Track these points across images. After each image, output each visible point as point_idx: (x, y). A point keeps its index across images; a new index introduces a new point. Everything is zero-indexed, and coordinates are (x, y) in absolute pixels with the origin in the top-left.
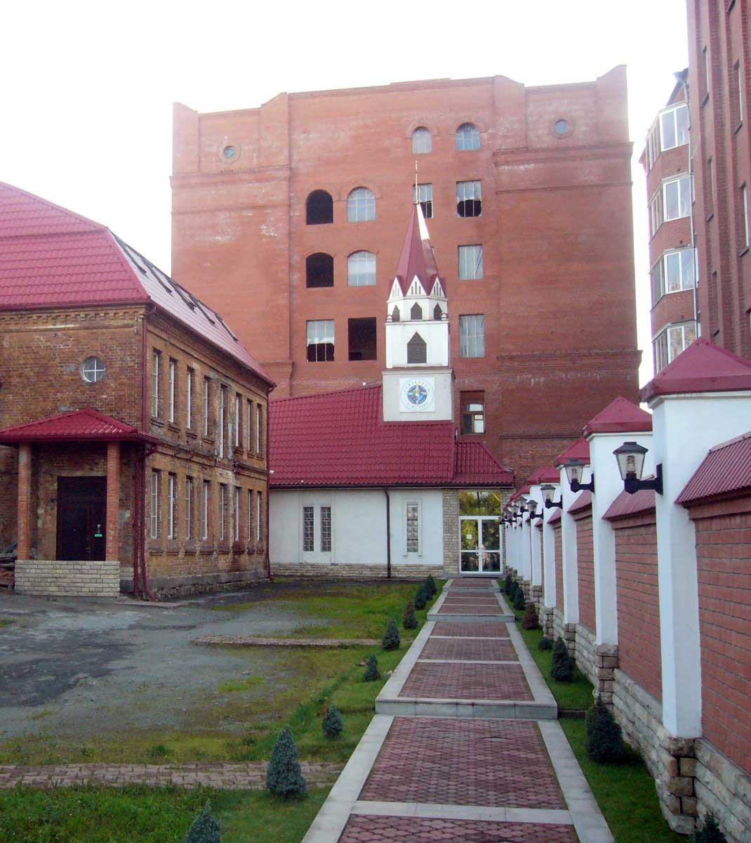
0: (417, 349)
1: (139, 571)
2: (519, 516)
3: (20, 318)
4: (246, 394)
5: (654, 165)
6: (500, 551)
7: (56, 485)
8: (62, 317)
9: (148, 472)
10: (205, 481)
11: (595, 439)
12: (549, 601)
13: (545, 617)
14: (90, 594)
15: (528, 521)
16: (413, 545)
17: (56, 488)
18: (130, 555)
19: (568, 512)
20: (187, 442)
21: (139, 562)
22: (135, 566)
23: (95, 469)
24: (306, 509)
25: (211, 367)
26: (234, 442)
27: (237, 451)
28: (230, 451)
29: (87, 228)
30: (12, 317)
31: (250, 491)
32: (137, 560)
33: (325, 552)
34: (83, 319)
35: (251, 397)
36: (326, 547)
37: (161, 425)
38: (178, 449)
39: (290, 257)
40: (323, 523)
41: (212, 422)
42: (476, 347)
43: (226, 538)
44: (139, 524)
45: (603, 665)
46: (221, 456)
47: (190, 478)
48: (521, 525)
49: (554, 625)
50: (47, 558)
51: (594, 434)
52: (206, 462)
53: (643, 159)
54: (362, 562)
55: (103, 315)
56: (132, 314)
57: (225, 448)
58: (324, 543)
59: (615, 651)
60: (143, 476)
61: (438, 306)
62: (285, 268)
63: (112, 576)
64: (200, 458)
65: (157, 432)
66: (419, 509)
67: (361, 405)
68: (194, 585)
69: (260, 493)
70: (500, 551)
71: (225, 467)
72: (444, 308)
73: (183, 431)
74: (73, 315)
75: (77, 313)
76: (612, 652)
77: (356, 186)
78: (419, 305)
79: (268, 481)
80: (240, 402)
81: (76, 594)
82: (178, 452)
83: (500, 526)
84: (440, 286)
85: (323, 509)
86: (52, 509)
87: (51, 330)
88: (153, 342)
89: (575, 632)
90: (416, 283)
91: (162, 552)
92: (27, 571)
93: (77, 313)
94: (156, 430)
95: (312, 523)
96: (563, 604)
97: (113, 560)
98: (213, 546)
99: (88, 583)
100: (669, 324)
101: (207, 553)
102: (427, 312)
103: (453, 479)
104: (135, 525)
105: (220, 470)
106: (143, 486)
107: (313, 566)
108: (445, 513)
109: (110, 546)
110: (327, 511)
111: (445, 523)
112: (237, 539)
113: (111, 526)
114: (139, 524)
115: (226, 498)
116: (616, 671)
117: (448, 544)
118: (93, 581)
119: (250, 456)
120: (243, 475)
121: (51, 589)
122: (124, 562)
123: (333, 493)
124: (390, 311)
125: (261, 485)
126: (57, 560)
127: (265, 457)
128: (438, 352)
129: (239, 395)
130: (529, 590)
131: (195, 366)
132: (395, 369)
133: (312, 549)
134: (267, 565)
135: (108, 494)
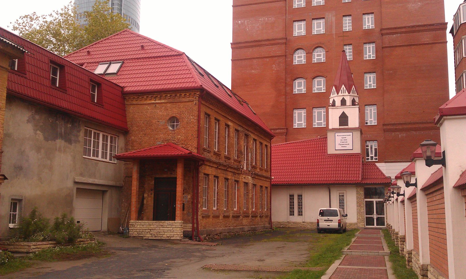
0: (344, 119)
1: (195, 226)
2: (392, 197)
3: (138, 98)
4: (259, 140)
5: (463, 75)
6: (385, 216)
7: (153, 181)
8: (158, 97)
9: (201, 175)
10: (235, 181)
12: (409, 246)
13: (407, 255)
14: (167, 238)
15: (397, 200)
17: (154, 183)
18: (190, 218)
19: (421, 189)
20: (225, 161)
21: (195, 221)
22: (193, 223)
23: (174, 174)
24: (290, 196)
25: (239, 125)
26: (252, 163)
27: (254, 167)
28: (250, 166)
29: (173, 53)
30: (134, 97)
31: (261, 187)
32: (194, 220)
34: (169, 98)
35: (261, 141)
36: (300, 214)
37: (209, 152)
38: (219, 164)
39: (286, 80)
40: (299, 203)
41: (240, 152)
42: (372, 120)
43: (248, 208)
44: (195, 201)
46: (245, 168)
47: (227, 179)
48: (393, 202)
49: (413, 260)
50: (148, 219)
51: (445, 117)
52: (236, 171)
53: (452, 32)
55: (179, 95)
56: (193, 94)
57: (247, 165)
58: (299, 212)
60: (198, 177)
61: (354, 99)
62: (284, 85)
63: (178, 229)
64: (232, 170)
65: (207, 155)
66: (345, 196)
67: (335, 163)
68: (229, 232)
69: (267, 188)
71: (246, 174)
72: (357, 100)
73: (222, 156)
74: (164, 95)
75: (166, 95)
79: (271, 182)
80: (256, 143)
81: (160, 238)
82: (218, 166)
84: (354, 89)
86: (151, 194)
87: (153, 103)
88: (204, 109)
90: (343, 88)
91: (209, 216)
92: (136, 226)
93: (166, 95)
94: (206, 154)
96: (418, 249)
97: (179, 220)
98: (240, 213)
99: (166, 232)
101: (236, 217)
102: (349, 102)
104: (193, 202)
105: (244, 176)
106: (198, 182)
109: (178, 212)
110: (300, 197)
112: (254, 210)
113: (179, 202)
114: (195, 201)
115: (247, 190)
117: (359, 213)
118: (169, 231)
119: (261, 169)
120: (207, 165)
121: (147, 235)
122: (185, 221)
124: (331, 101)
125: (267, 184)
126: (153, 220)
127: (269, 170)
128: (354, 122)
129: (255, 140)
131: (230, 123)
132: (334, 130)
133: (293, 215)
134: (270, 222)
135: (177, 186)
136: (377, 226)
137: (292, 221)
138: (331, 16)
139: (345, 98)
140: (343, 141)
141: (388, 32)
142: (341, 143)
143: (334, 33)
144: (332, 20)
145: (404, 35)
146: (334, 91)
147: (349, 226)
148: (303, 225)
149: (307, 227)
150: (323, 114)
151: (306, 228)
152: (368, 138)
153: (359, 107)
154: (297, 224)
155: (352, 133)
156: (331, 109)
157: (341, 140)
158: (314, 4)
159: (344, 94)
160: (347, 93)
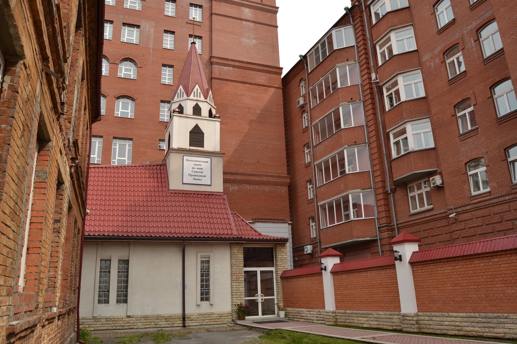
16: (205, 296)
33: (121, 305)
72: (214, 112)
78: (199, 126)
90: (181, 90)
100: (346, 146)
102: (205, 112)
107: (107, 319)
133: (107, 302)
136: (262, 315)
137: (103, 315)
138: (147, 26)
139: (200, 104)
140: (196, 170)
141: (219, 62)
142: (192, 174)
143: (152, 47)
144: (149, 31)
145: (236, 69)
146: (182, 92)
147: (218, 319)
148: (128, 323)
149: (136, 327)
150: (127, 148)
151: (133, 328)
154: (114, 322)
155: (211, 158)
156: (177, 118)
157: (193, 168)
158: (128, 5)
159: (198, 98)
160: (202, 98)
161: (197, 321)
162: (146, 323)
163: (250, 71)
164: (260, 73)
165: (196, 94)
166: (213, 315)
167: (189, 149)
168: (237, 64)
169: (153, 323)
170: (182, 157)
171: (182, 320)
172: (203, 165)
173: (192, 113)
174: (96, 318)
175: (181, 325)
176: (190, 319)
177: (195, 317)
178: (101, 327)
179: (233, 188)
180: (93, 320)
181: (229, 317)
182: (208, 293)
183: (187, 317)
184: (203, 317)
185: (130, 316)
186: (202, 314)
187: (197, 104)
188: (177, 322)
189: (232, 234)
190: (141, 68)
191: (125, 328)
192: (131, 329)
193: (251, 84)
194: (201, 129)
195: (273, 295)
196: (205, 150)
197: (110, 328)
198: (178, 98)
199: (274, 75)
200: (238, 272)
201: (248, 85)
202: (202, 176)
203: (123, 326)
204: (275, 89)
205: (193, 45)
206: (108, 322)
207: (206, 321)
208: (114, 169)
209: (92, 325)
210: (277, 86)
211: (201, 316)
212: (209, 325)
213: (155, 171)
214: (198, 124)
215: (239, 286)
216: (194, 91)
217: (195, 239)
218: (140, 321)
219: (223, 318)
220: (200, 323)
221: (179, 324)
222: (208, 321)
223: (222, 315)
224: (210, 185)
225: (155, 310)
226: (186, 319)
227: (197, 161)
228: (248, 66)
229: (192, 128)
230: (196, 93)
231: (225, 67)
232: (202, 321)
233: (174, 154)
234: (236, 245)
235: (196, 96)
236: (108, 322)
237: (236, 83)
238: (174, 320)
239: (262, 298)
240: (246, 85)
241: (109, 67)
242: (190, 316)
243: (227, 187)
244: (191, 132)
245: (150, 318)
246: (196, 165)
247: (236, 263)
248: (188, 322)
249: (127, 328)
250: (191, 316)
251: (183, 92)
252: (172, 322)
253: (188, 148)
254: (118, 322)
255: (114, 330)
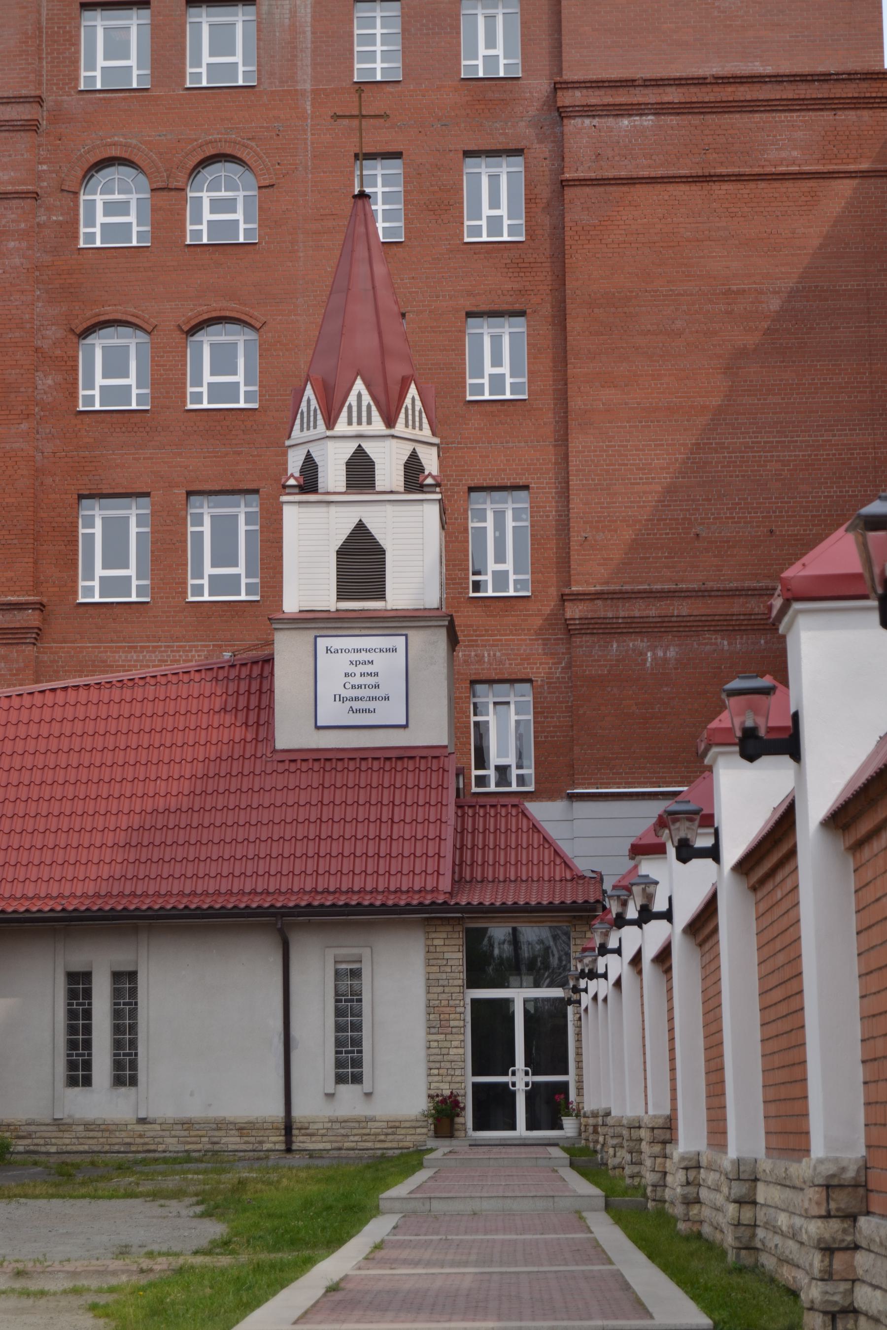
11: (802, 622)
33: (123, 1090)
40: (117, 1014)
45: (829, 1211)
54: (215, 1113)
58: (118, 1065)
59: (858, 1171)
70: (571, 1078)
72: (430, 461)
76: (850, 1174)
77: (211, 151)
78: (369, 526)
83: (570, 1009)
84: (418, 404)
85: (117, 976)
89: (756, 1180)
90: (359, 396)
95: (88, 1015)
103: (451, 894)
107: (88, 1126)
108: (430, 984)
111: (430, 1008)
116: (863, 1221)
123: (282, 1036)
130: (641, 1140)
133: (87, 1081)
139: (370, 448)
140: (357, 681)
141: (593, 101)
143: (308, 87)
145: (672, 120)
146: (312, 408)
147: (387, 1134)
148: (141, 1136)
152: (486, 666)
153: (440, 501)
154: (107, 1134)
155: (406, 636)
157: (347, 675)
159: (364, 429)
160: (378, 425)
161: (325, 1139)
162: (188, 1139)
163: (738, 116)
164: (783, 115)
165: (355, 414)
166: (373, 1123)
167: (337, 610)
168: (673, 95)
169: (206, 1139)
170: (312, 640)
171: (283, 1132)
172: (381, 662)
173: (344, 484)
174: (60, 1122)
175: (282, 1147)
176: (308, 1131)
177: (320, 1126)
178: (74, 1144)
179: (660, 653)
180: (54, 1128)
181: (419, 1131)
182: (357, 1063)
183: (299, 1125)
184: (343, 1128)
185: (145, 1119)
186: (340, 1119)
187: (360, 451)
188: (270, 1138)
189: (435, 890)
190: (271, 190)
191: (133, 1148)
192: (149, 1151)
193: (738, 178)
194: (376, 536)
195: (566, 1073)
196: (389, 608)
197: (96, 1149)
198: (302, 430)
199: (852, 113)
200: (444, 1003)
201: (725, 186)
202: (375, 699)
203: (130, 1144)
204: (855, 182)
205: (360, 202)
206: (91, 1134)
207: (352, 1138)
208: (122, 688)
209: (53, 1140)
210: (864, 166)
211: (337, 1126)
212: (360, 1150)
213: (243, 687)
214: (364, 521)
215: (447, 1044)
216: (347, 404)
217: (310, 910)
218: (173, 1133)
219: (403, 1131)
220: (335, 1145)
221: (275, 1143)
222: (356, 1138)
223: (397, 1124)
224: (405, 726)
225: (210, 1105)
226: (295, 1132)
227: (359, 651)
228: (728, 93)
229: (345, 537)
230: (355, 409)
231: (619, 120)
232: (340, 1138)
233: (287, 633)
234: (439, 922)
235: (355, 419)
236: (91, 1134)
237: (670, 187)
238: (261, 1133)
239: (514, 1079)
240: (715, 187)
241: (149, 202)
242: (306, 1125)
243: (634, 650)
244: (341, 553)
245: (197, 1126)
246: (357, 663)
247: (439, 976)
248: (301, 1138)
249: (140, 1149)
250: (309, 1123)
251: (315, 410)
252: (258, 1139)
253: (333, 609)
254: (117, 1133)
255: (106, 1152)
